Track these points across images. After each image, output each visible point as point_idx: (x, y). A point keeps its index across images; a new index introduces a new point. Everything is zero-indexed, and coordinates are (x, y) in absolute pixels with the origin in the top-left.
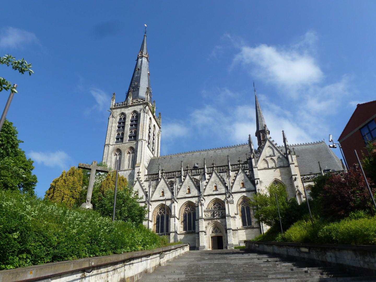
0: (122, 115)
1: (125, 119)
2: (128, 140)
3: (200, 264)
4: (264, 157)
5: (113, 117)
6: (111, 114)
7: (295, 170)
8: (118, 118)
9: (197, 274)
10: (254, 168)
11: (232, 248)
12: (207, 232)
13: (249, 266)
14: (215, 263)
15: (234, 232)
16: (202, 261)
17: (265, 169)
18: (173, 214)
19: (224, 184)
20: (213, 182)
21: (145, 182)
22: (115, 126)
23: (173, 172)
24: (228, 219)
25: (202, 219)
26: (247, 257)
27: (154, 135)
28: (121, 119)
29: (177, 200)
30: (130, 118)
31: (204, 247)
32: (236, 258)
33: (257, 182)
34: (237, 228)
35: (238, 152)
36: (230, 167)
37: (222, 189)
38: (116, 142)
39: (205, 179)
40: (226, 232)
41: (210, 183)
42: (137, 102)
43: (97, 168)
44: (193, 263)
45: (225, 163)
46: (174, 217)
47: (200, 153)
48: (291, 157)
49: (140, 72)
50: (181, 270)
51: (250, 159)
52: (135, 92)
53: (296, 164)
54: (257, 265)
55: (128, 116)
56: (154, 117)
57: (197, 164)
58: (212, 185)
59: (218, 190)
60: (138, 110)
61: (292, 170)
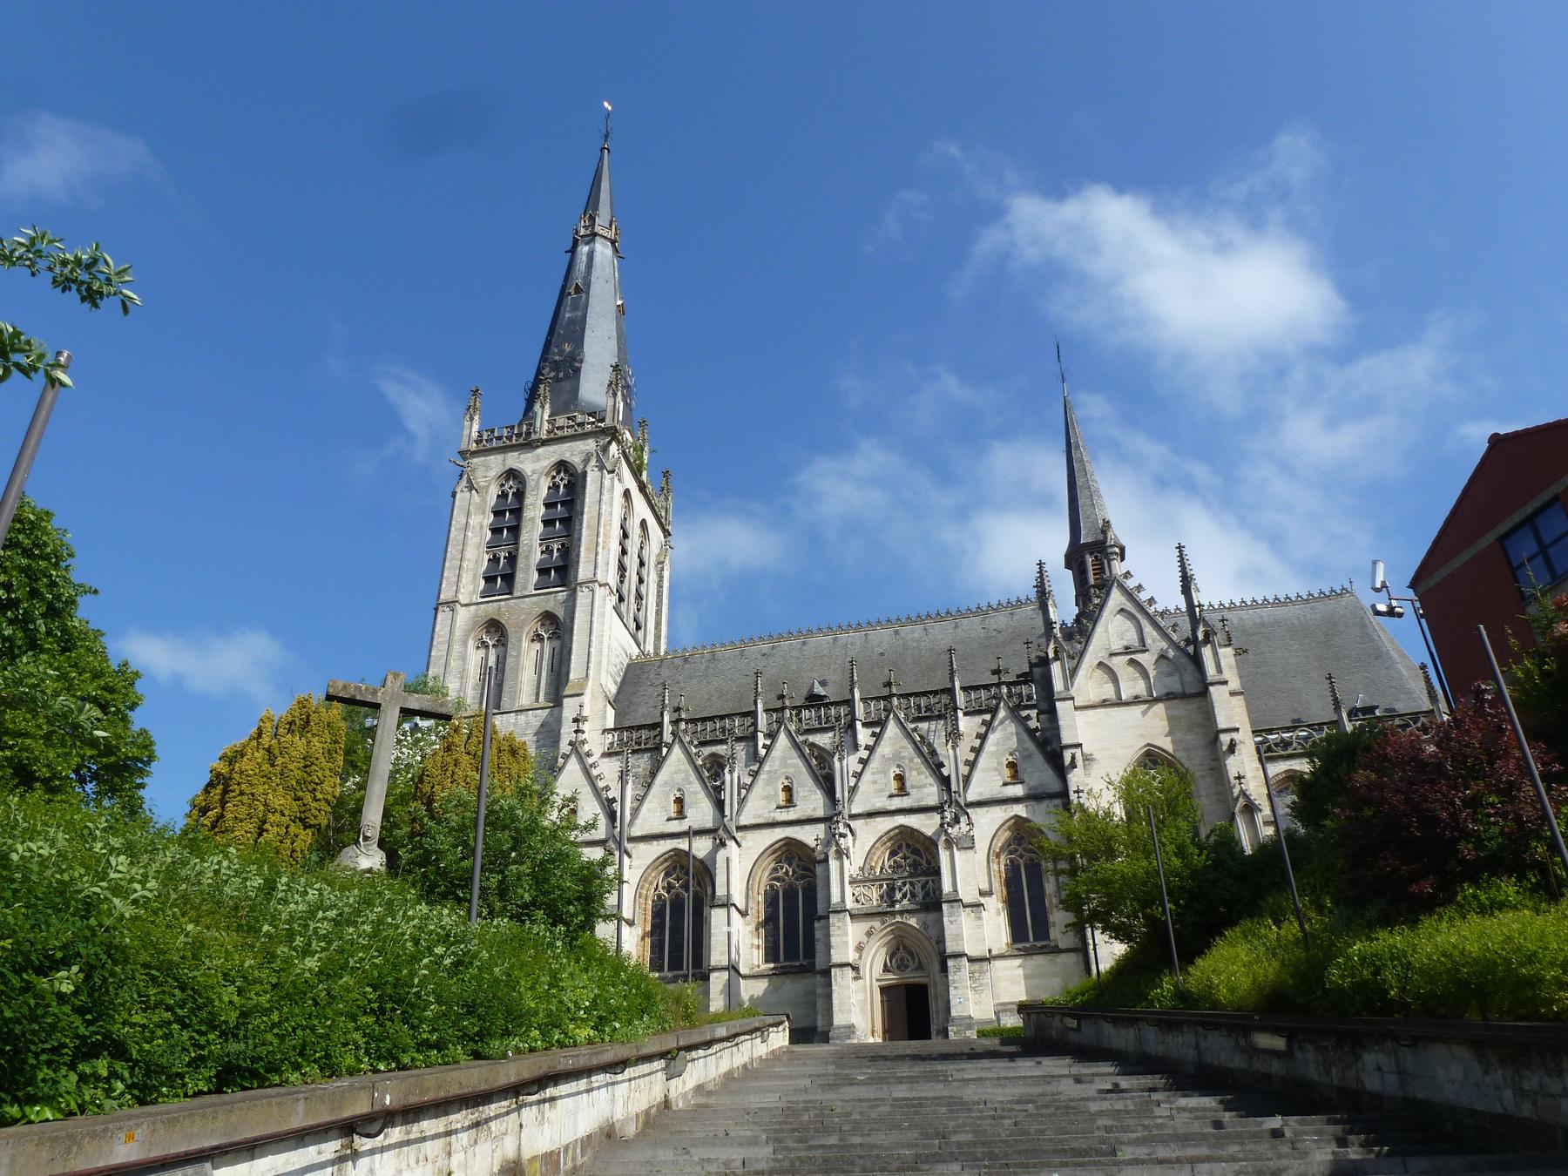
0: (507, 480)
1: (520, 495)
5: (471, 487)
6: (461, 476)
7: (1230, 710)
8: (494, 491)
10: (1059, 700)
11: (968, 1033)
12: (864, 968)
13: (1037, 1108)
14: (895, 1095)
15: (977, 966)
17: (1105, 704)
20: (887, 760)
21: (606, 760)
22: (481, 526)
23: (722, 717)
24: (951, 915)
25: (841, 915)
27: (642, 564)
28: (503, 496)
29: (738, 835)
30: (544, 492)
31: (851, 1029)
32: (982, 1074)
33: (1073, 757)
34: (990, 951)
35: (995, 633)
36: (961, 698)
39: (856, 747)
40: (944, 969)
41: (875, 763)
42: (573, 426)
43: (405, 700)
44: (808, 1097)
46: (727, 904)
48: (1215, 654)
49: (583, 299)
51: (1044, 662)
52: (562, 384)
53: (1235, 684)
56: (642, 488)
57: (823, 684)
60: (576, 460)
61: (1216, 710)
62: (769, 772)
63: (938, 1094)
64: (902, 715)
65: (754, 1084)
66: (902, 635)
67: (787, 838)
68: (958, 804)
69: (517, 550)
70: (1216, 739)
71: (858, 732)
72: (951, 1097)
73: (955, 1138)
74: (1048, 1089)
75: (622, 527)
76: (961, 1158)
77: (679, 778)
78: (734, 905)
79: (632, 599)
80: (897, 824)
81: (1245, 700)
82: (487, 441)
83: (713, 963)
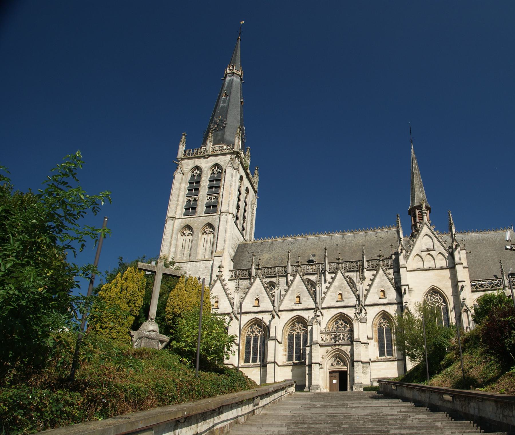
1: (200, 176)
2: (205, 212)
3: (308, 413)
7: (463, 274)
8: (190, 174)
9: (302, 427)
10: (401, 268)
11: (360, 389)
13: (372, 418)
14: (329, 412)
15: (365, 365)
16: (311, 410)
17: (418, 270)
19: (355, 290)
20: (337, 287)
21: (230, 281)
23: (275, 267)
24: (356, 346)
27: (246, 205)
28: (193, 176)
29: (279, 313)
30: (209, 176)
31: (318, 386)
32: (359, 405)
33: (405, 290)
34: (370, 359)
35: (380, 239)
36: (366, 265)
38: (184, 214)
39: (325, 281)
40: (353, 366)
41: (332, 289)
42: (221, 150)
43: (165, 270)
44: (299, 412)
45: (357, 257)
46: (275, 339)
47: (319, 238)
48: (459, 253)
49: (228, 99)
51: (397, 254)
52: (218, 132)
53: (465, 264)
56: (247, 174)
57: (314, 256)
58: (335, 292)
59: (343, 301)
60: (222, 164)
61: (458, 274)
62: (292, 290)
63: (343, 412)
65: (282, 406)
67: (297, 315)
68: (362, 305)
69: (198, 198)
70: (457, 284)
71: (326, 275)
74: (379, 411)
75: (244, 208)
76: (343, 432)
77: (257, 291)
78: (277, 340)
82: (188, 154)
83: (268, 360)
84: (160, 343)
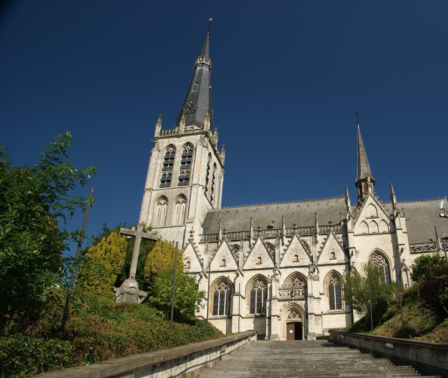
1: (174, 153)
2: (178, 184)
4: (364, 219)
7: (402, 238)
8: (165, 151)
9: (263, 371)
10: (349, 233)
11: (313, 338)
12: (282, 317)
13: (323, 363)
14: (286, 358)
15: (317, 317)
16: (271, 356)
17: (364, 234)
18: (237, 290)
19: (308, 252)
21: (200, 245)
23: (239, 232)
24: (310, 301)
26: (326, 352)
27: (214, 178)
28: (168, 153)
29: (243, 272)
30: (182, 153)
31: (277, 336)
33: (352, 252)
34: (322, 312)
35: (331, 208)
36: (318, 230)
37: (305, 260)
38: (160, 186)
39: (283, 244)
40: (307, 318)
41: (289, 251)
42: (193, 130)
43: (143, 235)
44: (260, 358)
45: (311, 224)
46: (239, 295)
47: (278, 207)
48: (399, 220)
49: (198, 86)
50: (246, 366)
51: (345, 221)
52: (190, 115)
53: (405, 230)
54: (333, 362)
55: (178, 149)
56: (215, 151)
57: (273, 222)
58: (292, 254)
59: (299, 261)
60: (193, 142)
61: (398, 238)
62: (254, 252)
64: (298, 235)
65: (245, 353)
66: (300, 207)
68: (315, 265)
69: (172, 172)
70: (398, 247)
71: (284, 239)
72: (302, 359)
73: (298, 370)
75: (212, 181)
76: (299, 376)
77: (224, 253)
78: (241, 295)
79: (210, 190)
80: (295, 271)
81: (408, 236)
83: (234, 313)
84: (139, 299)
